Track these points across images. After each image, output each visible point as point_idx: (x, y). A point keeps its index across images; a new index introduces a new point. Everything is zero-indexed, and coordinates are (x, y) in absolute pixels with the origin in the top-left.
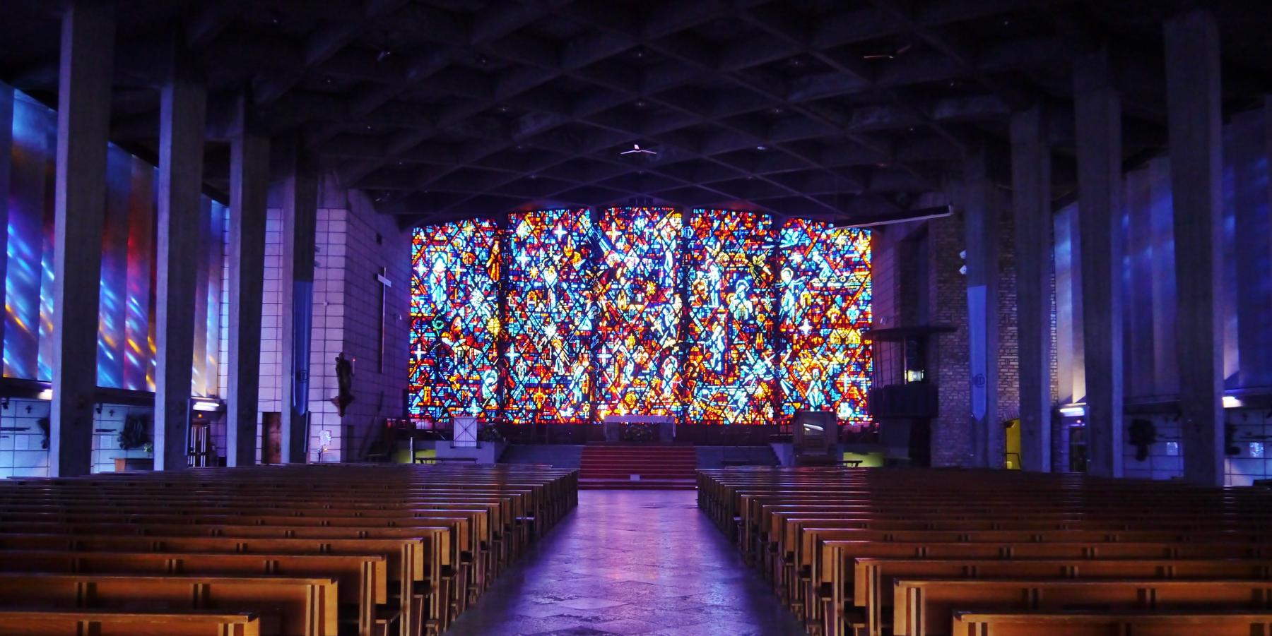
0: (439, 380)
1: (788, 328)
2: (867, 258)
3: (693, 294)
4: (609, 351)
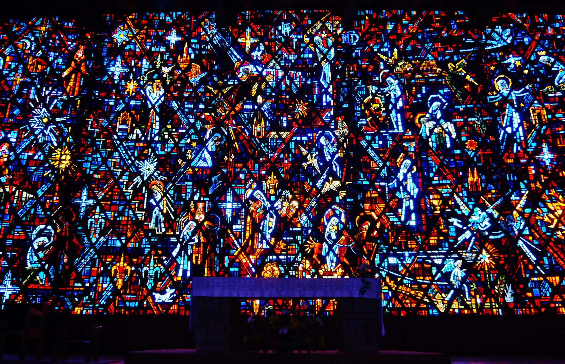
1: (517, 157)
3: (364, 116)
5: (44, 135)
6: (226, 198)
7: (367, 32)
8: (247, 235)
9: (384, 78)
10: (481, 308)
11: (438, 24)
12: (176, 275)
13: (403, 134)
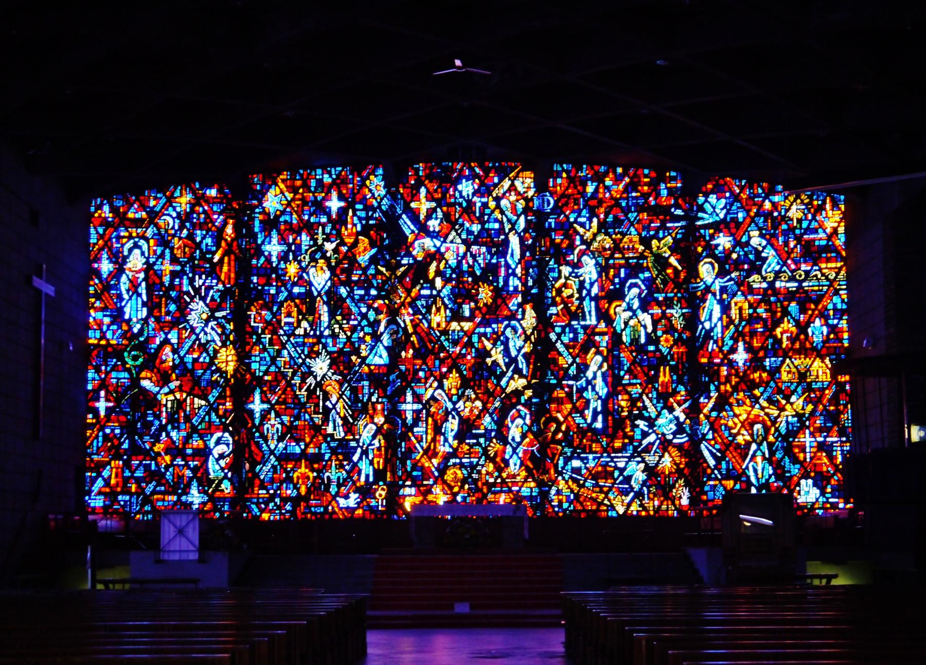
0: (136, 450)
1: (711, 356)
2: (840, 241)
3: (555, 304)
5: (206, 334)
6: (405, 399)
7: (563, 195)
8: (429, 438)
9: (580, 257)
10: (657, 510)
11: (646, 188)
12: (359, 480)
13: (596, 326)
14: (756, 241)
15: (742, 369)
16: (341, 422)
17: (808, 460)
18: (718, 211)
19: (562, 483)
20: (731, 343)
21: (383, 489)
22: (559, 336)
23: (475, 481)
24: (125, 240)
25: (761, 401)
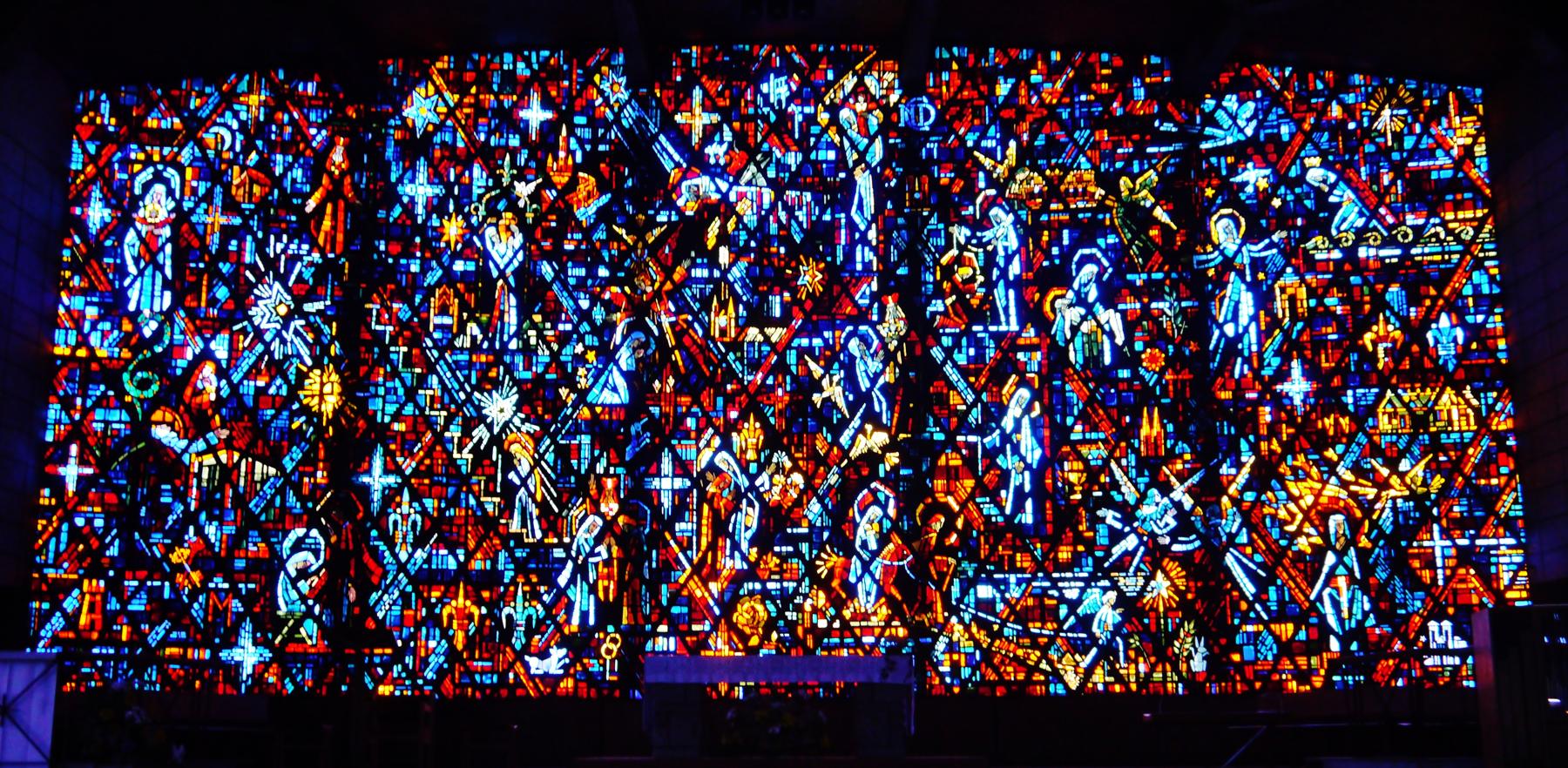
0: (133, 560)
1: (1239, 387)
2: (1479, 170)
3: (940, 294)
4: (682, 468)
5: (284, 342)
7: (953, 100)
10: (1144, 682)
11: (1105, 86)
12: (568, 622)
13: (1018, 334)
14: (1316, 175)
15: (1300, 410)
16: (535, 512)
17: (1441, 583)
18: (1241, 123)
19: (959, 628)
20: (1276, 362)
21: (614, 641)
22: (948, 352)
23: (791, 626)
24: (137, 167)
25: (1341, 470)
